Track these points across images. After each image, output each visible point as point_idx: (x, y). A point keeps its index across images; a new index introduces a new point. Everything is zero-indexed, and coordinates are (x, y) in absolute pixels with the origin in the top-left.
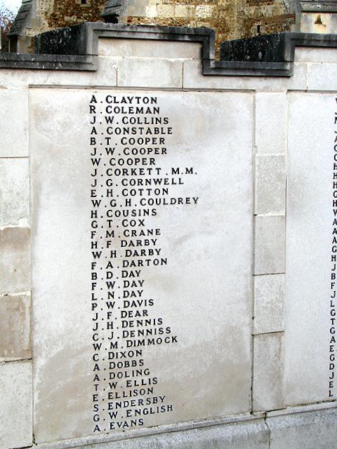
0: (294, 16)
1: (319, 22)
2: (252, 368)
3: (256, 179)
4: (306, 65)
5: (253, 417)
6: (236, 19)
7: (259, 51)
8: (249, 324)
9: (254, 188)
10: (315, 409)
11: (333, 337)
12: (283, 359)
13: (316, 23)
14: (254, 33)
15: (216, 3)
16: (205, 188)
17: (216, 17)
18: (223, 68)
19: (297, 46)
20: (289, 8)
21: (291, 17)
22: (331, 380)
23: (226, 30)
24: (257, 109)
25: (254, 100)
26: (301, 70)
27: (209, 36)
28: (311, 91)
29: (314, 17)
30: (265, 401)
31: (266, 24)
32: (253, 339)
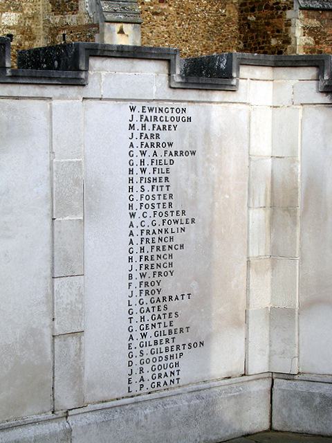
0: (97, 26)
1: (121, 32)
2: (54, 368)
3: (54, 184)
4: (100, 74)
5: (55, 416)
6: (41, 27)
7: (55, 60)
8: (50, 326)
9: (52, 193)
10: (115, 405)
11: (131, 336)
12: (84, 358)
13: (118, 33)
14: (59, 41)
15: (22, 11)
16: (4, 193)
17: (22, 25)
18: (19, 76)
19: (91, 56)
20: (93, 18)
21: (95, 27)
22: (130, 377)
23: (32, 38)
24: (53, 117)
25: (51, 107)
26: (96, 78)
27: (4, 45)
28: (106, 99)
29: (117, 27)
30: (66, 399)
31: (71, 32)
32: (53, 340)
